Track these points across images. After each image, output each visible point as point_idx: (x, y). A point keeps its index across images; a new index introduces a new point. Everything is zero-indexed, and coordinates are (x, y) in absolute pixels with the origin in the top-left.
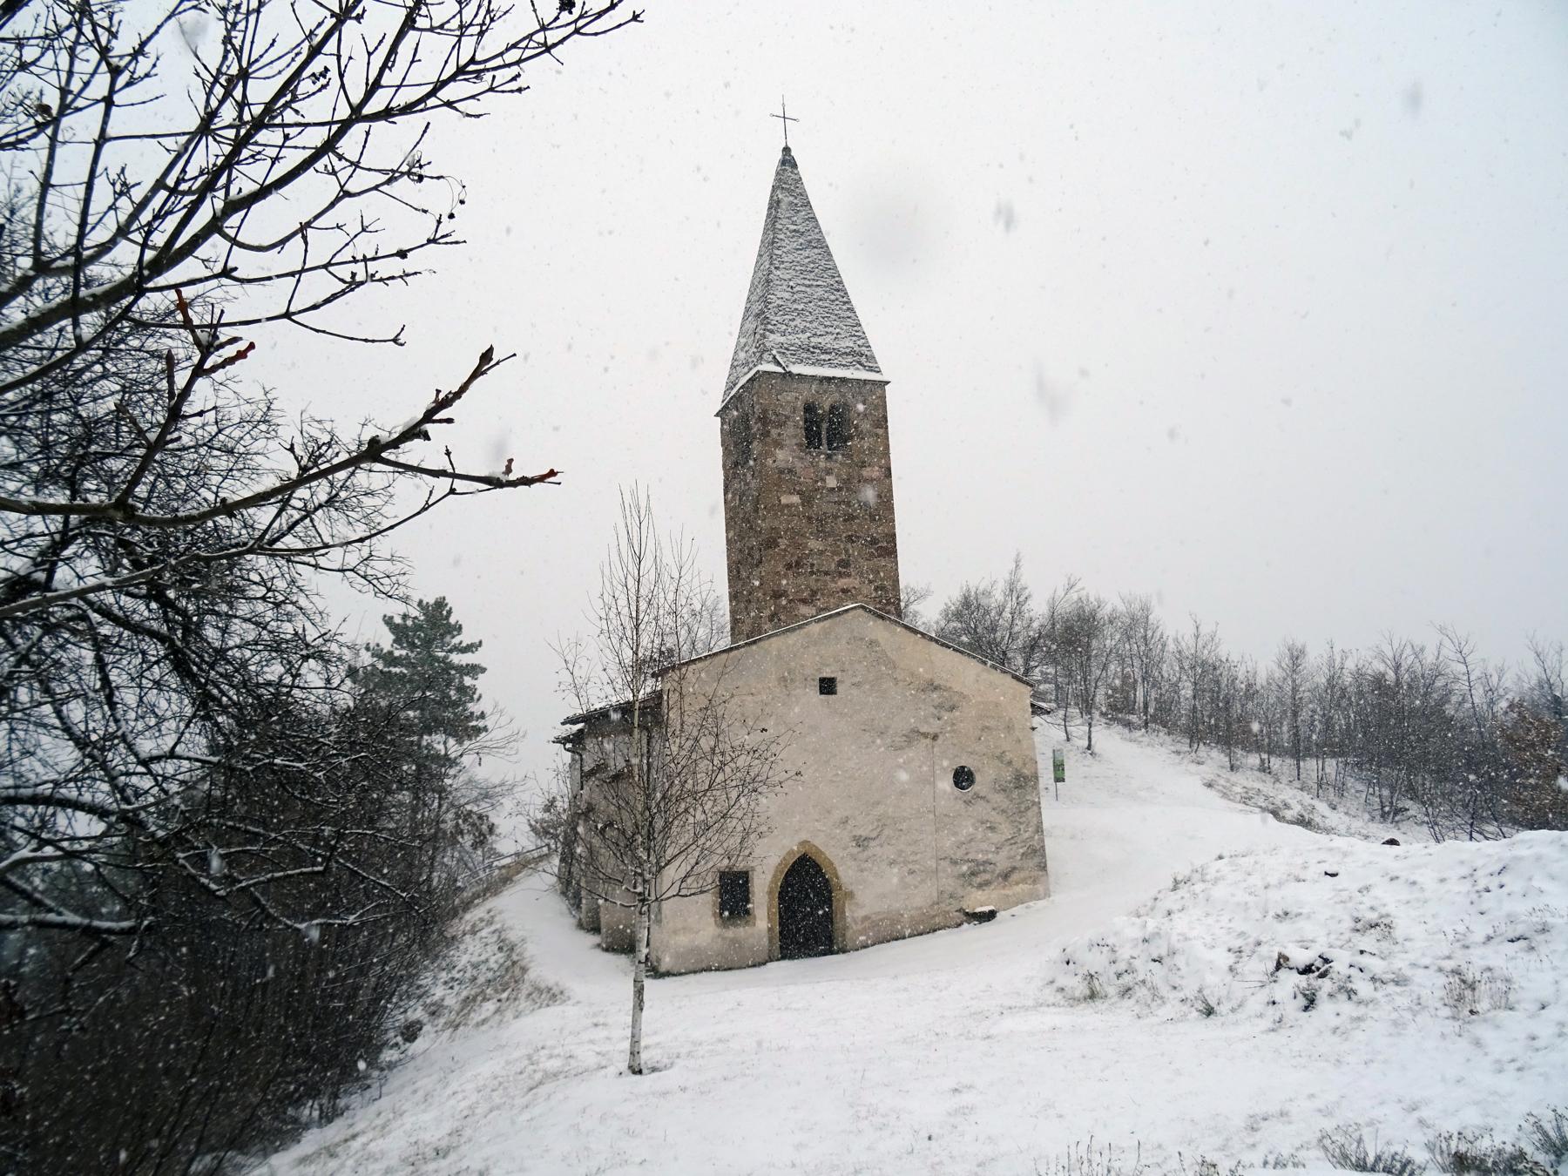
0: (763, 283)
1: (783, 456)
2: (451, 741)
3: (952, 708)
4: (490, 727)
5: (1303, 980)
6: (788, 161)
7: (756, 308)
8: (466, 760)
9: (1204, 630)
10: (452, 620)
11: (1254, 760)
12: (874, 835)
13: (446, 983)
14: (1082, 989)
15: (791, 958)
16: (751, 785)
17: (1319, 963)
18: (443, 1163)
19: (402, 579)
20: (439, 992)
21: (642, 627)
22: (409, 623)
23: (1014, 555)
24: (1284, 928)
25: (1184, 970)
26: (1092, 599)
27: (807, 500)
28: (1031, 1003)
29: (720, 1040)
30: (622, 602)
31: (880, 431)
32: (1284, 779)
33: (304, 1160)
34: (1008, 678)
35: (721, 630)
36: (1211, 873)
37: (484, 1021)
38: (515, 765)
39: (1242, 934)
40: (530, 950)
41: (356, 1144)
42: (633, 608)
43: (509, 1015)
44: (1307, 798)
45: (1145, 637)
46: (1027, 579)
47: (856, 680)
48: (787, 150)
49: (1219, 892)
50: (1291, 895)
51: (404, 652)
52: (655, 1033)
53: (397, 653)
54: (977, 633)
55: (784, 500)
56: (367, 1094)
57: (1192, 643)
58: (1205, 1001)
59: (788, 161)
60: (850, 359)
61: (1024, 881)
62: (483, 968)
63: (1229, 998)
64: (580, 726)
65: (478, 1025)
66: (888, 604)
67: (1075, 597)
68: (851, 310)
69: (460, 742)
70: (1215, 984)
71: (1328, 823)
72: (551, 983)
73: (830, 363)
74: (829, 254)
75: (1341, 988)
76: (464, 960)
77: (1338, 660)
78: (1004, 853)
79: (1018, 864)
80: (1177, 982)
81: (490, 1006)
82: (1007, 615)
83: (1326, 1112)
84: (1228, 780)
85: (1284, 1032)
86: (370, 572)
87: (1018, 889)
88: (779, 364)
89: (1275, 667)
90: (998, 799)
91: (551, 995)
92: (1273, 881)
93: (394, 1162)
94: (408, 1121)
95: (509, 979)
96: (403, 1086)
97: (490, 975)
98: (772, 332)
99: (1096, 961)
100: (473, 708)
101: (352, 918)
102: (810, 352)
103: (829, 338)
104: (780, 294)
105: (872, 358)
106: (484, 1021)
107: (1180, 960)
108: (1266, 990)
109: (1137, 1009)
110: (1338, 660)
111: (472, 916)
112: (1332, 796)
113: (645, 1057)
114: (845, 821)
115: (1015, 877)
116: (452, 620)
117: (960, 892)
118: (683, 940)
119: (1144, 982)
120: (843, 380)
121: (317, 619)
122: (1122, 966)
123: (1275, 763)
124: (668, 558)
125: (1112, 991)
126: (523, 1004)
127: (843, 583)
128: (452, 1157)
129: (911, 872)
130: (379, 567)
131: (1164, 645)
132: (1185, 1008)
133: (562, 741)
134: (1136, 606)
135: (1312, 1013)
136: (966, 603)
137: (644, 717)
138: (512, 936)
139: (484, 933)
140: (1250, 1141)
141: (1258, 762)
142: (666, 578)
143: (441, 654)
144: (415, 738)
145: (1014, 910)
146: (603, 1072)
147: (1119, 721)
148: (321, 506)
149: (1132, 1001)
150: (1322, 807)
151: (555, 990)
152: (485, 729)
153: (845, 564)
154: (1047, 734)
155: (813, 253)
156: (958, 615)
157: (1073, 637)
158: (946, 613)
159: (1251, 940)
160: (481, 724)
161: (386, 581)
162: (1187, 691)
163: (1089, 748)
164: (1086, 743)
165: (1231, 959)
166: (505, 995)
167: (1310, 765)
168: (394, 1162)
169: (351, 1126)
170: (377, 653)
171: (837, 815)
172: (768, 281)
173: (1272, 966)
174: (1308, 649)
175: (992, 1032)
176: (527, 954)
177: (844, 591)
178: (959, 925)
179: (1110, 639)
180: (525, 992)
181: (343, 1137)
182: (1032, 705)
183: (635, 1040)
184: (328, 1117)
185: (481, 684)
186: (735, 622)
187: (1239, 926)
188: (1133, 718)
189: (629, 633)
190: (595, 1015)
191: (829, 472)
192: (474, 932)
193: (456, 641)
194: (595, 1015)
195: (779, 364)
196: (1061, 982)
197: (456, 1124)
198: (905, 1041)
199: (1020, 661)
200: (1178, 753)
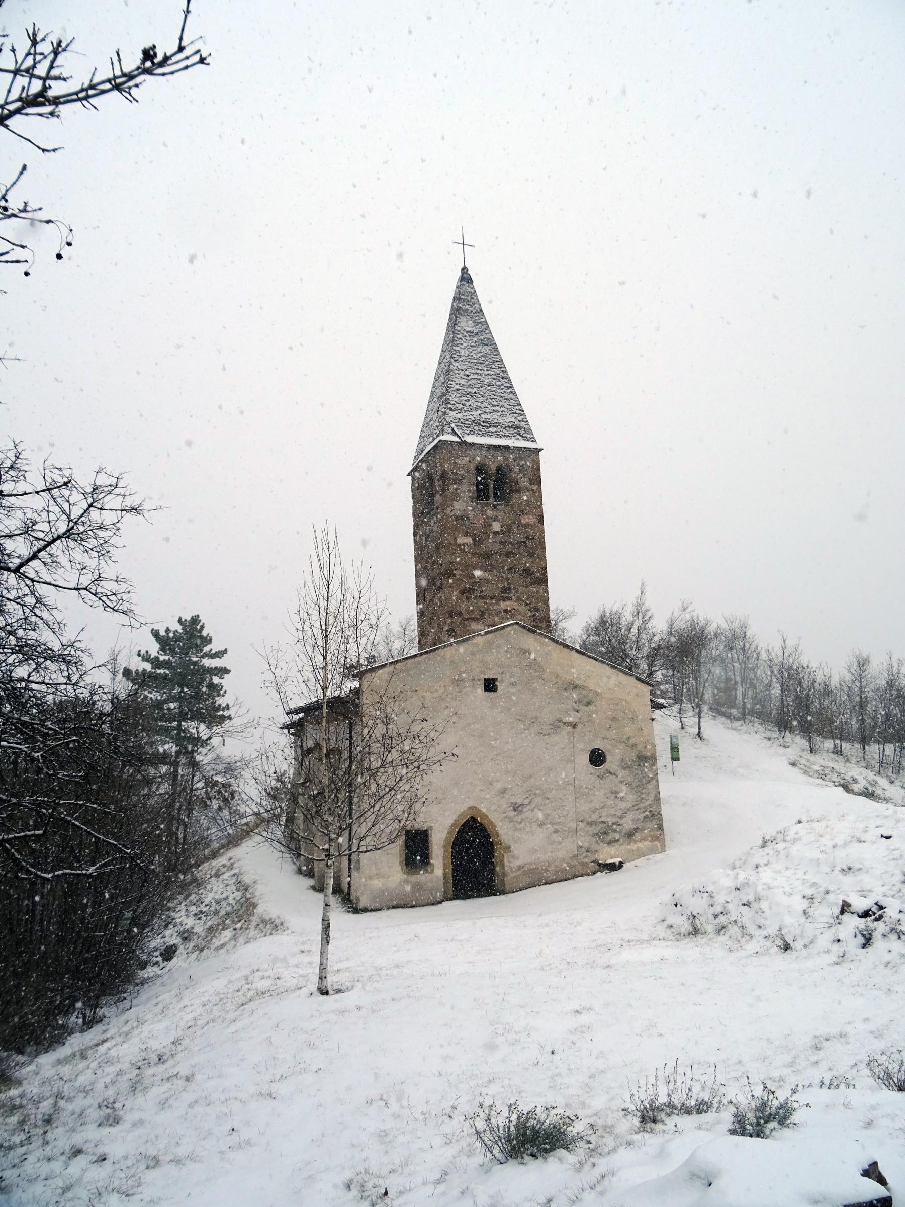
0: (445, 372)
1: (458, 507)
2: (202, 727)
3: (588, 703)
4: (232, 716)
5: (862, 923)
6: (466, 278)
7: (439, 392)
8: (215, 741)
9: (789, 643)
10: (204, 633)
11: (829, 744)
12: (526, 802)
13: (195, 915)
14: (686, 927)
15: (466, 897)
16: (415, 764)
17: (875, 909)
18: (161, 1068)
19: (125, 597)
20: (189, 922)
21: (330, 636)
22: (171, 635)
23: (640, 585)
24: (848, 879)
25: (768, 913)
26: (701, 619)
27: (477, 541)
28: (645, 937)
29: (397, 966)
30: (315, 616)
31: (535, 488)
32: (853, 760)
33: (59, 1062)
34: (633, 680)
35: (411, 640)
36: (791, 835)
37: (223, 946)
38: (252, 743)
39: (814, 884)
40: (260, 890)
41: (102, 1049)
42: (323, 622)
43: (241, 940)
44: (871, 775)
45: (743, 649)
46: (649, 602)
47: (513, 680)
48: (465, 270)
49: (795, 850)
50: (854, 854)
51: (167, 658)
52: (347, 959)
53: (162, 658)
54: (610, 644)
55: (459, 541)
56: (121, 1005)
57: (780, 653)
58: (783, 939)
59: (466, 278)
60: (512, 431)
61: (643, 839)
62: (224, 904)
63: (802, 937)
64: (301, 715)
65: (218, 949)
66: (540, 622)
67: (688, 617)
68: (514, 393)
69: (209, 727)
70: (792, 924)
71: (887, 794)
72: (274, 916)
73: (499, 436)
74: (496, 349)
75: (892, 930)
76: (209, 898)
77: (895, 665)
78: (631, 815)
79: (640, 825)
80: (762, 922)
81: (227, 934)
82: (634, 630)
83: (878, 1034)
84: (808, 761)
85: (847, 965)
86: (99, 590)
87: (640, 845)
88: (455, 434)
89: (845, 672)
90: (621, 773)
91: (273, 926)
92: (840, 842)
93: (125, 1066)
94: (146, 1028)
95: (243, 913)
96: (149, 999)
97: (229, 909)
98: (451, 409)
99: (698, 904)
100: (220, 701)
101: (91, 869)
102: (486, 426)
103: (495, 415)
104: (458, 380)
105: (529, 431)
106: (223, 946)
107: (764, 905)
108: (833, 930)
109: (729, 943)
110: (895, 665)
111: (217, 863)
112: (890, 774)
113: (332, 980)
114: (504, 791)
115: (638, 836)
116: (204, 633)
117: (595, 847)
118: (377, 883)
119: (735, 922)
120: (507, 448)
121: (56, 627)
122: (718, 909)
123: (846, 746)
124: (351, 583)
125: (710, 928)
126: (252, 933)
127: (503, 605)
128: (170, 1063)
129: (556, 831)
130: (108, 587)
131: (758, 655)
132: (768, 944)
133: (288, 727)
134: (736, 624)
135: (870, 949)
136: (603, 621)
137: (343, 709)
138: (247, 879)
139: (225, 876)
140: (814, 1058)
141: (832, 746)
142: (349, 598)
143: (195, 659)
144: (175, 724)
145: (637, 862)
146: (298, 992)
147: (723, 714)
148: (59, 537)
149: (726, 937)
150: (883, 782)
151: (277, 922)
152: (230, 718)
153: (506, 590)
154: (665, 725)
155: (486, 349)
156: (597, 631)
157: (685, 651)
158: (588, 631)
159: (822, 890)
160: (226, 713)
161: (113, 598)
162: (776, 691)
163: (699, 734)
164: (697, 731)
165: (805, 904)
166: (239, 926)
167: (874, 749)
168: (125, 1066)
169: (105, 1031)
170: (146, 658)
171: (499, 786)
172: (449, 371)
173: (837, 910)
174: (871, 659)
175: (612, 962)
176: (257, 893)
177: (506, 611)
178: (594, 873)
179: (716, 648)
180: (254, 923)
181: (94, 1042)
182: (652, 701)
183: (323, 967)
184: (89, 1024)
185: (226, 682)
186: (422, 634)
187: (812, 877)
188: (734, 711)
189: (320, 642)
190: (303, 943)
191: (495, 519)
192: (217, 875)
193: (206, 649)
194: (303, 943)
195: (455, 434)
196: (670, 921)
197: (180, 1033)
198: (542, 969)
199: (644, 666)
200: (769, 739)
